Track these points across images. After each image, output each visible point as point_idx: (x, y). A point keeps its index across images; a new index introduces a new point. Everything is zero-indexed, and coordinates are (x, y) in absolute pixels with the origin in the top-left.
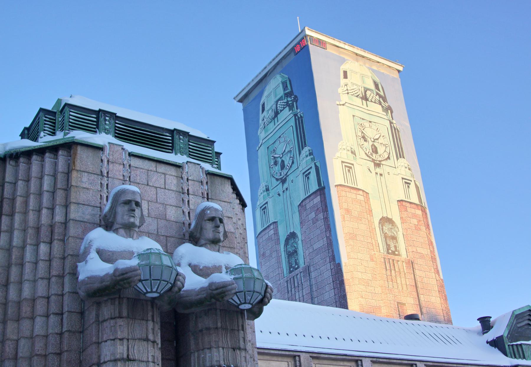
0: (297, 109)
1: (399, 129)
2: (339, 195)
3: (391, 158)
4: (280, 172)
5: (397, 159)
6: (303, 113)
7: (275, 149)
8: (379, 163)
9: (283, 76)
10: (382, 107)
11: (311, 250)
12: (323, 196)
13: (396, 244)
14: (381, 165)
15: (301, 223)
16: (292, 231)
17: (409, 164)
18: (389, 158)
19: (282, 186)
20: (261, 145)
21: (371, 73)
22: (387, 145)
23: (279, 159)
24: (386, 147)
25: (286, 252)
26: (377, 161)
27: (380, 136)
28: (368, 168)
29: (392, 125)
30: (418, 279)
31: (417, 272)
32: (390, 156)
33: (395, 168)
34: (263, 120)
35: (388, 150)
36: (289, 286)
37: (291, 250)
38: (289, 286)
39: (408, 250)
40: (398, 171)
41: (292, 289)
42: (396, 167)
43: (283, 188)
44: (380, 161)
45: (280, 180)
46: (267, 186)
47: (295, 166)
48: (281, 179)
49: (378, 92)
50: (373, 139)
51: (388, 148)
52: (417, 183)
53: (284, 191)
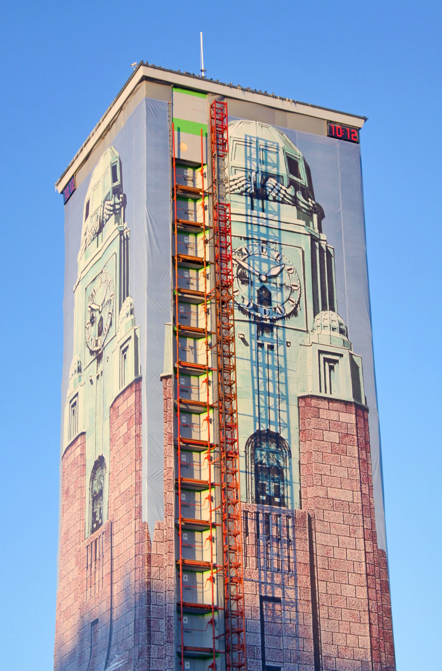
0: (124, 222)
1: (331, 251)
2: (168, 396)
3: (299, 312)
4: (97, 339)
5: (316, 312)
6: (129, 231)
7: (94, 293)
8: (271, 325)
9: (113, 151)
10: (299, 209)
11: (117, 494)
12: (138, 393)
13: (279, 483)
14: (275, 330)
15: (111, 440)
16: (101, 455)
17: (342, 321)
18: (294, 313)
19: (97, 366)
20: (79, 282)
21: (286, 142)
22: (297, 286)
23: (97, 312)
24: (292, 291)
25: (92, 491)
26: (266, 319)
27: (281, 271)
28: (241, 336)
29: (317, 244)
30: (319, 551)
31: (319, 538)
32: (298, 309)
33: (307, 331)
34: (86, 234)
35: (295, 297)
36: (89, 556)
37: (96, 489)
38: (89, 556)
39: (306, 493)
40: (313, 337)
41: (92, 563)
42: (310, 329)
43: (97, 369)
44: (272, 320)
45: (95, 353)
46: (80, 363)
47: (112, 329)
48: (97, 351)
49: (295, 178)
50: (266, 276)
51: (297, 294)
52: (355, 358)
53: (98, 376)
